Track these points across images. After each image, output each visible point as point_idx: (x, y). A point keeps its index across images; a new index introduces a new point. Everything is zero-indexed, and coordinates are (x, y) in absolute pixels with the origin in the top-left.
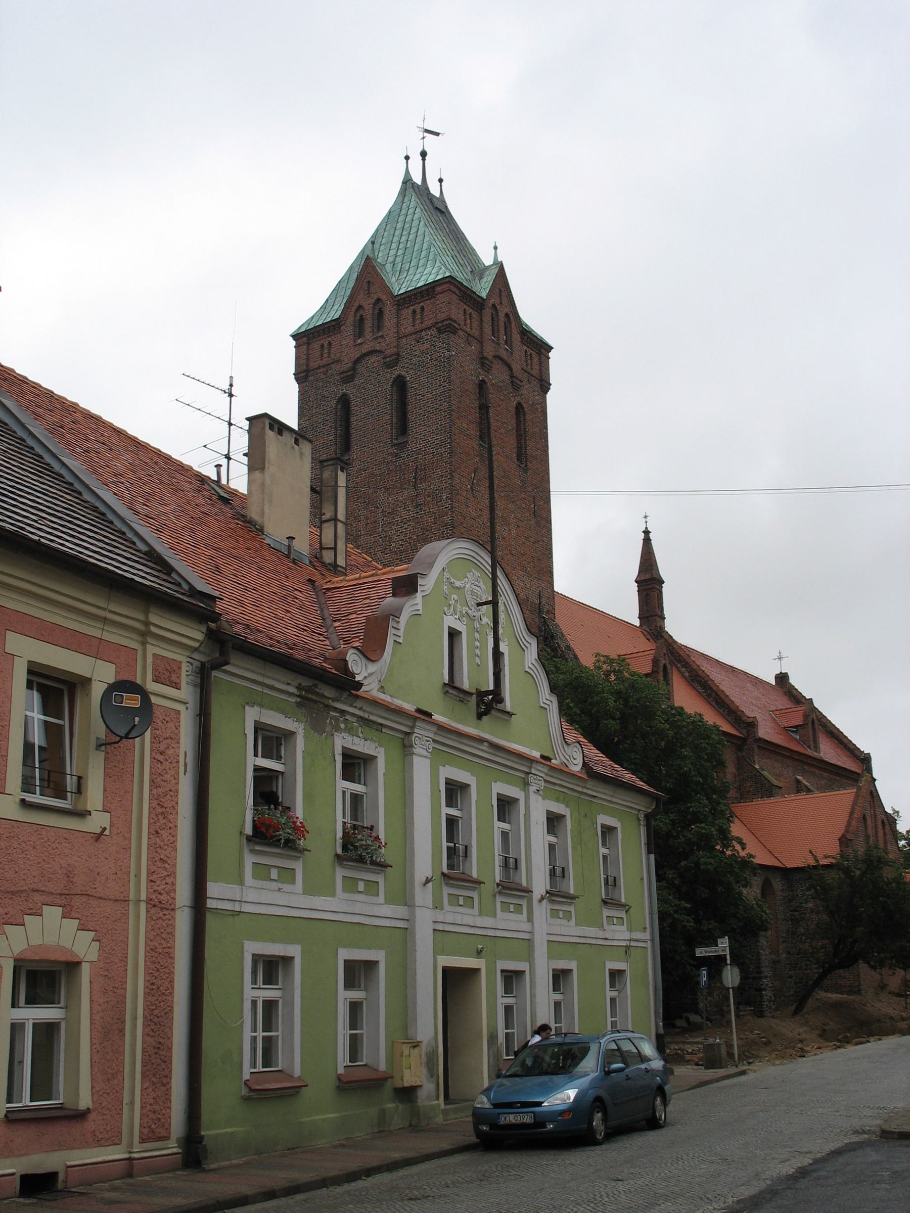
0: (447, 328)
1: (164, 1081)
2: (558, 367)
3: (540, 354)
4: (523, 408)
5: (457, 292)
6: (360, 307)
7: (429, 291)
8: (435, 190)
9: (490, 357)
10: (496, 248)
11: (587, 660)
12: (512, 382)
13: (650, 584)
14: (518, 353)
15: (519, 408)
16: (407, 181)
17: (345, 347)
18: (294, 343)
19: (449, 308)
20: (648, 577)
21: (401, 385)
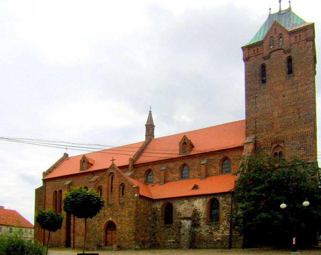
20: (150, 124)
21: (289, 60)
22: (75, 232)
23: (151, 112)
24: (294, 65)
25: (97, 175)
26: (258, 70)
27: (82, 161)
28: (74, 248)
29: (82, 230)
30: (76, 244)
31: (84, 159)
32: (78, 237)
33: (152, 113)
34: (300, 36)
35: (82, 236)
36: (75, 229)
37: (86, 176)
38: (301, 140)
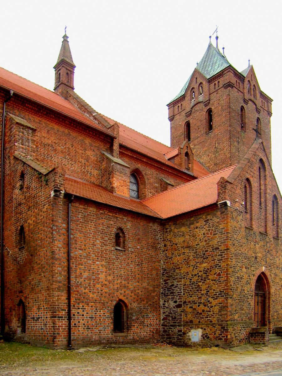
0: (229, 85)
1: (146, 325)
2: (275, 107)
3: (268, 102)
4: (259, 119)
5: (233, 72)
6: (193, 88)
7: (220, 74)
8: (221, 51)
9: (247, 99)
10: (249, 61)
11: (190, 334)
12: (257, 110)
13: (65, 68)
14: (259, 101)
15: (258, 119)
16: (210, 46)
17: (187, 105)
18: (167, 108)
19: (229, 77)
21: (210, 111)
22: (73, 288)
23: (67, 37)
24: (263, 230)
25: (16, 111)
26: (182, 129)
28: (69, 346)
29: (98, 286)
30: (79, 332)
32: (84, 309)
33: (68, 40)
34: (219, 82)
35: (98, 305)
36: (73, 280)
38: (245, 250)
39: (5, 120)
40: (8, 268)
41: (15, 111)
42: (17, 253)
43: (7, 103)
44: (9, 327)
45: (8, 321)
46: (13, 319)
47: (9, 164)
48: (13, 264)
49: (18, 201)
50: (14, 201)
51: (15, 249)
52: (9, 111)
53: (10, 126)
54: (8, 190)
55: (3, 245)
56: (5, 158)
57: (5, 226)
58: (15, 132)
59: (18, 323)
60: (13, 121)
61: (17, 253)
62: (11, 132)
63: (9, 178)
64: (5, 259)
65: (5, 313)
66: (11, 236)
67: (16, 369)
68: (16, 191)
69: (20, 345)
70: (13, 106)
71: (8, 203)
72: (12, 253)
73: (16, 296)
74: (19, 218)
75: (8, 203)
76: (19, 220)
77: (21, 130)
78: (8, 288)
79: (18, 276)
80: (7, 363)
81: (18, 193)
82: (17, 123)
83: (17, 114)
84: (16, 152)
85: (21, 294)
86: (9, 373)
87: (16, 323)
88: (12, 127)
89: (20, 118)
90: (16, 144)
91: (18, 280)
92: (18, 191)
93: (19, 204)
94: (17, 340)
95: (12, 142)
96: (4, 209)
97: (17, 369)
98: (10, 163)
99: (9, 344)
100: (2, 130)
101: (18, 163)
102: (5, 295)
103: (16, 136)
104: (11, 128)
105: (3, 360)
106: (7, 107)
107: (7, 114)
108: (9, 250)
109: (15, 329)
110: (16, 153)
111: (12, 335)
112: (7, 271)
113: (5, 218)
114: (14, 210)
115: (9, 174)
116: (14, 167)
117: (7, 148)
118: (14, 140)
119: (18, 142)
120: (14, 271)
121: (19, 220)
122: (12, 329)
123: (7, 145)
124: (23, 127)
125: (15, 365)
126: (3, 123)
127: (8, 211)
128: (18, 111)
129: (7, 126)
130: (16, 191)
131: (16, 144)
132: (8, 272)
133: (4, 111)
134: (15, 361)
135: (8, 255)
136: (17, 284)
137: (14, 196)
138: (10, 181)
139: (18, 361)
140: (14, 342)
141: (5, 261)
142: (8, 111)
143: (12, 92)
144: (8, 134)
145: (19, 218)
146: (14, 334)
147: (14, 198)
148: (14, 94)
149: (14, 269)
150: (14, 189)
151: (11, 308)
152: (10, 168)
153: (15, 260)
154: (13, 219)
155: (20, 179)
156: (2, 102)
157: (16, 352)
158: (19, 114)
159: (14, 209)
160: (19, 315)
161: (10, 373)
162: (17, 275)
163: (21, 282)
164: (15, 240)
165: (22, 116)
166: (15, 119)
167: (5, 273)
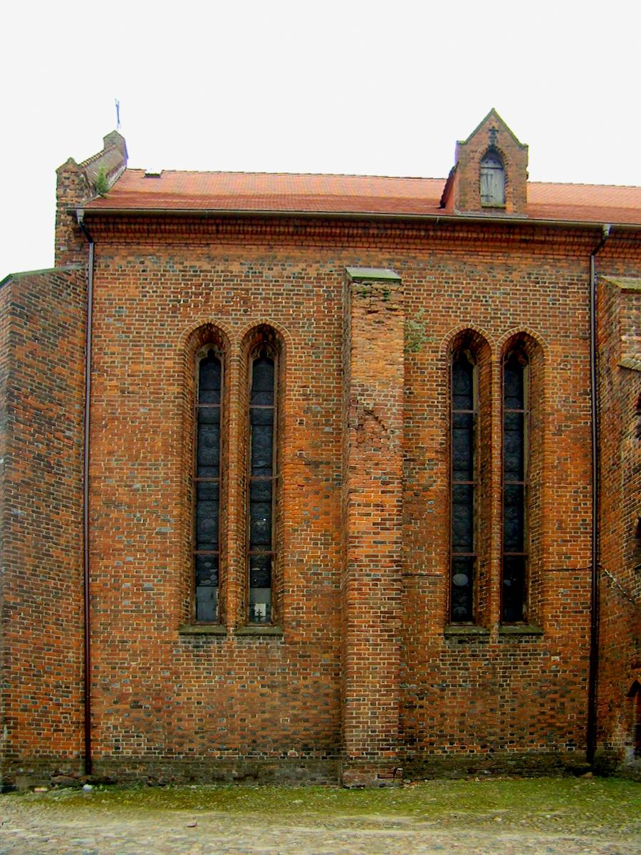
25: (619, 265)
27: (482, 148)
31: (493, 138)
37: (523, 264)
39: (595, 292)
40: (608, 616)
41: (616, 267)
42: (631, 580)
43: (597, 255)
44: (606, 745)
45: (604, 732)
46: (616, 727)
47: (608, 388)
48: (621, 605)
49: (632, 464)
50: (624, 465)
51: (626, 571)
52: (602, 270)
53: (607, 302)
54: (609, 444)
55: (597, 566)
56: (600, 375)
57: (602, 524)
58: (619, 313)
59: (628, 735)
60: (615, 290)
61: (631, 580)
62: (610, 316)
63: (611, 417)
64: (602, 596)
65: (598, 715)
66: (617, 544)
67: (626, 839)
68: (628, 442)
69: (631, 785)
70: (612, 257)
71: (608, 472)
72: (618, 581)
73: (625, 675)
74: (637, 501)
75: (608, 472)
76: (635, 504)
77: (634, 302)
78: (607, 659)
79: (631, 631)
80: (605, 822)
81: (632, 446)
82: (624, 291)
83: (621, 271)
84: (624, 355)
85: (636, 670)
86: (611, 846)
87: (622, 735)
88: (613, 303)
89: (628, 279)
90: (623, 338)
91: (630, 639)
92: (632, 440)
93: (634, 470)
94: (624, 775)
95: (614, 335)
96: (600, 488)
97: (630, 840)
98: (611, 383)
99: (605, 782)
100: (590, 317)
101: (630, 379)
102: (599, 674)
103: (621, 320)
104: (610, 307)
105: (595, 816)
106: (597, 264)
107: (598, 278)
108: (611, 576)
109: (619, 749)
110: (626, 358)
111: (612, 762)
112: (605, 622)
113: (603, 506)
114: (624, 485)
115: (609, 408)
116: (621, 390)
117: (603, 354)
118: (619, 331)
119: (627, 333)
120: (621, 620)
121: (635, 504)
122: (612, 748)
123: (603, 347)
124: (636, 295)
125: (624, 828)
126: (590, 301)
127: (608, 489)
128: (624, 262)
129: (601, 306)
130: (628, 442)
131: (623, 338)
132: (608, 625)
133: (593, 274)
134: (623, 821)
135: (609, 586)
136: (628, 649)
137: (623, 455)
138: (613, 424)
139: (631, 821)
140: (617, 777)
141: (601, 601)
142: (600, 273)
143: (607, 228)
144: (603, 322)
145: (637, 501)
146: (616, 759)
147: (623, 458)
148: (611, 231)
149: (621, 616)
150: (621, 440)
151: (612, 702)
152: (611, 394)
153: (625, 595)
154: (621, 505)
155: (637, 414)
156: (587, 256)
157: (622, 799)
158: (625, 270)
159: (623, 483)
160: (631, 716)
161: (615, 847)
162: (628, 630)
163: (637, 643)
164: (625, 551)
165: (633, 272)
166: (618, 284)
167: (601, 626)
